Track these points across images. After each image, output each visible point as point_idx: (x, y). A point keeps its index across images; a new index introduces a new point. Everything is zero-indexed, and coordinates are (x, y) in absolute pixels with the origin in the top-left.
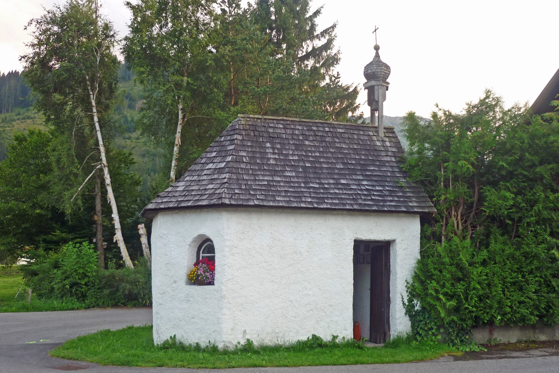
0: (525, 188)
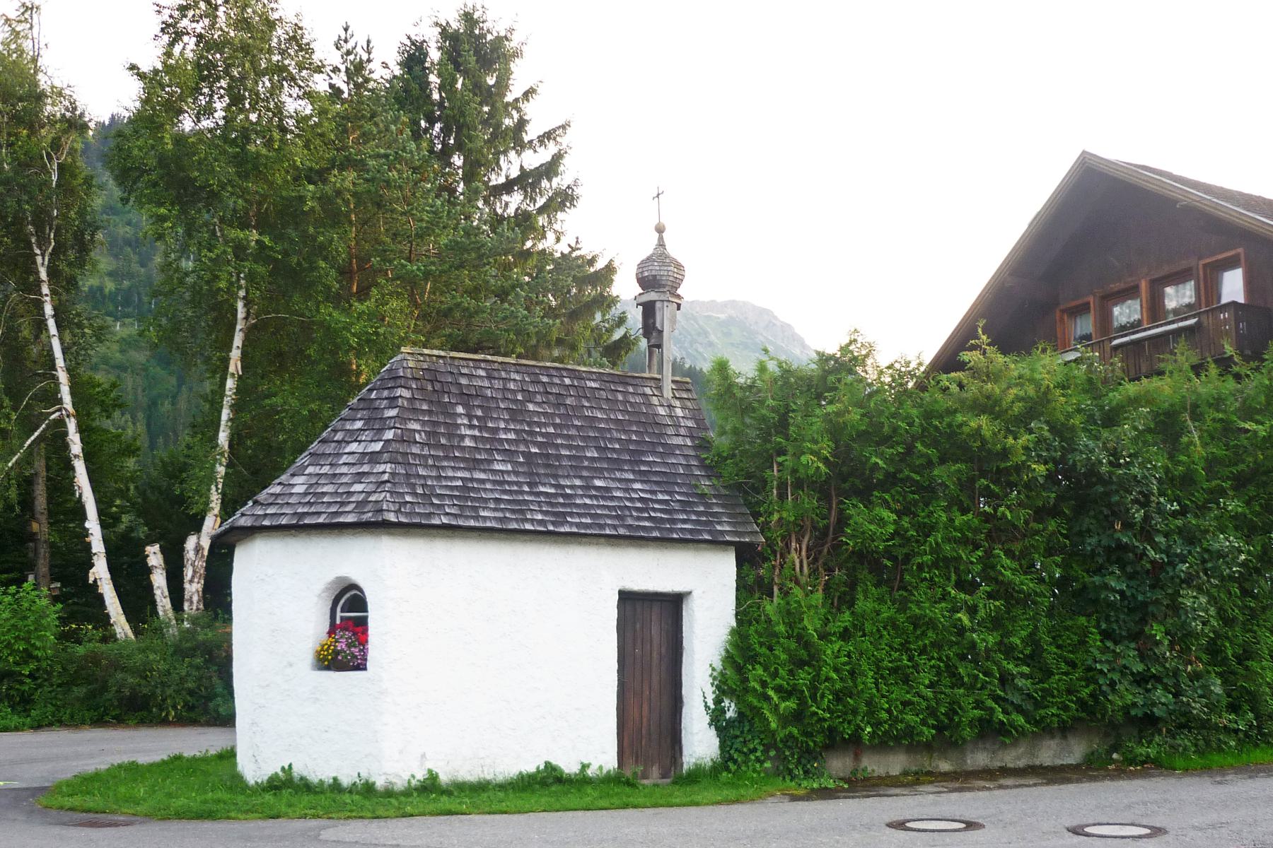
0: (915, 503)
